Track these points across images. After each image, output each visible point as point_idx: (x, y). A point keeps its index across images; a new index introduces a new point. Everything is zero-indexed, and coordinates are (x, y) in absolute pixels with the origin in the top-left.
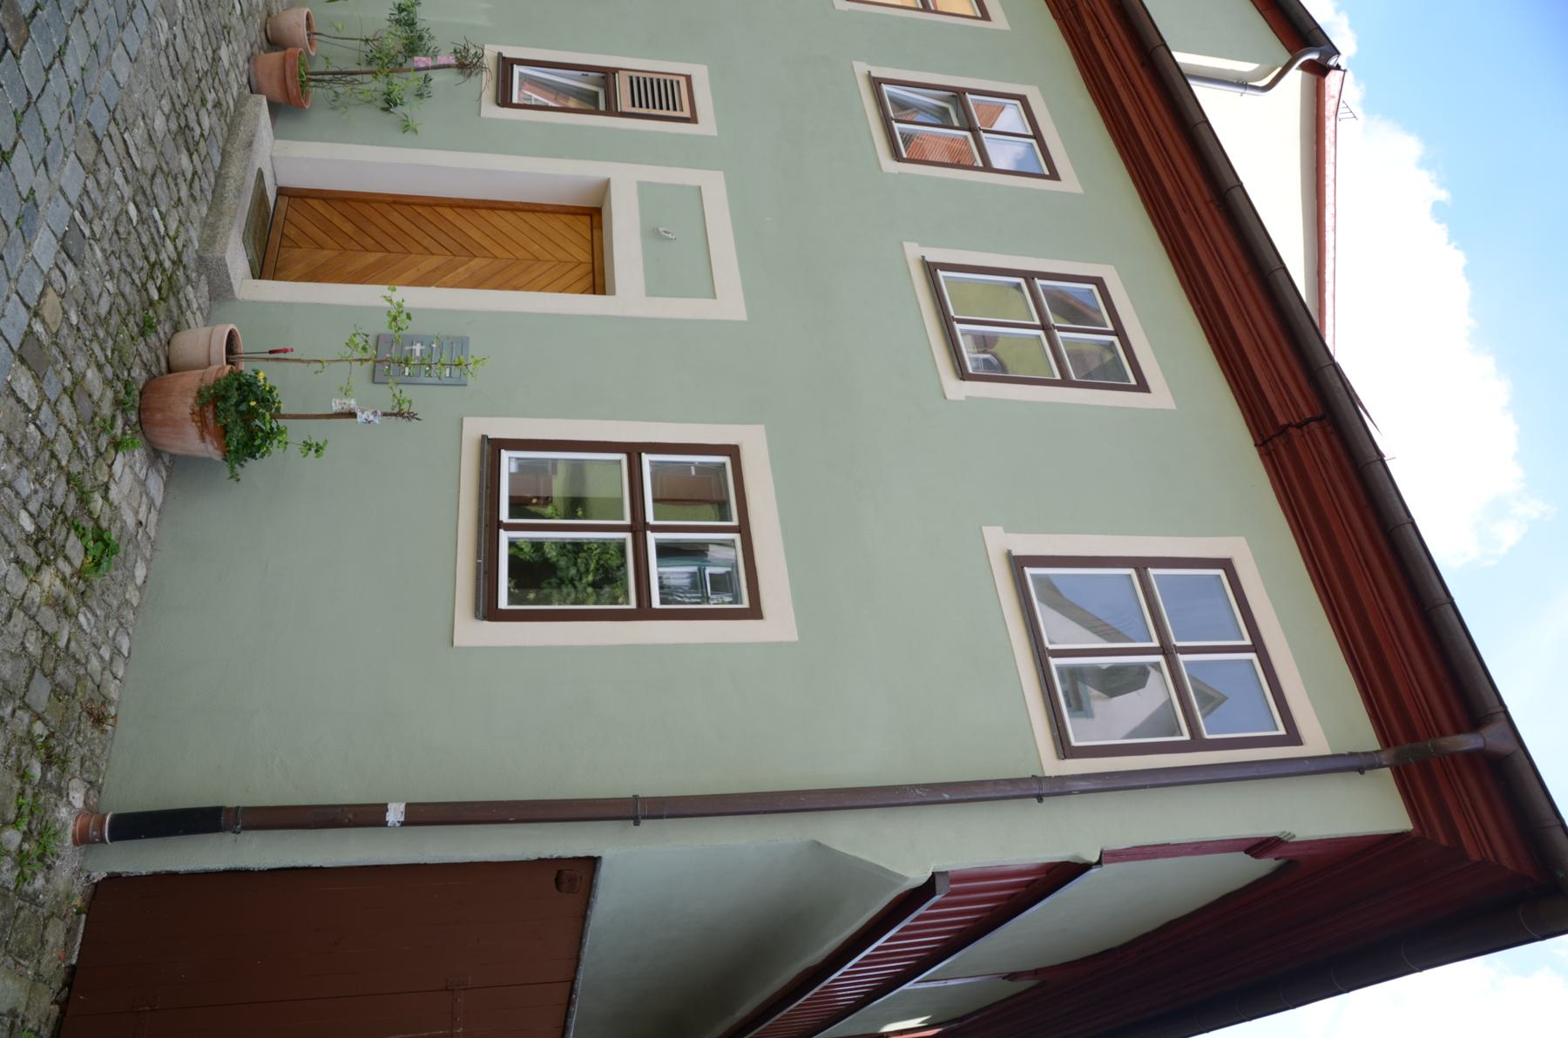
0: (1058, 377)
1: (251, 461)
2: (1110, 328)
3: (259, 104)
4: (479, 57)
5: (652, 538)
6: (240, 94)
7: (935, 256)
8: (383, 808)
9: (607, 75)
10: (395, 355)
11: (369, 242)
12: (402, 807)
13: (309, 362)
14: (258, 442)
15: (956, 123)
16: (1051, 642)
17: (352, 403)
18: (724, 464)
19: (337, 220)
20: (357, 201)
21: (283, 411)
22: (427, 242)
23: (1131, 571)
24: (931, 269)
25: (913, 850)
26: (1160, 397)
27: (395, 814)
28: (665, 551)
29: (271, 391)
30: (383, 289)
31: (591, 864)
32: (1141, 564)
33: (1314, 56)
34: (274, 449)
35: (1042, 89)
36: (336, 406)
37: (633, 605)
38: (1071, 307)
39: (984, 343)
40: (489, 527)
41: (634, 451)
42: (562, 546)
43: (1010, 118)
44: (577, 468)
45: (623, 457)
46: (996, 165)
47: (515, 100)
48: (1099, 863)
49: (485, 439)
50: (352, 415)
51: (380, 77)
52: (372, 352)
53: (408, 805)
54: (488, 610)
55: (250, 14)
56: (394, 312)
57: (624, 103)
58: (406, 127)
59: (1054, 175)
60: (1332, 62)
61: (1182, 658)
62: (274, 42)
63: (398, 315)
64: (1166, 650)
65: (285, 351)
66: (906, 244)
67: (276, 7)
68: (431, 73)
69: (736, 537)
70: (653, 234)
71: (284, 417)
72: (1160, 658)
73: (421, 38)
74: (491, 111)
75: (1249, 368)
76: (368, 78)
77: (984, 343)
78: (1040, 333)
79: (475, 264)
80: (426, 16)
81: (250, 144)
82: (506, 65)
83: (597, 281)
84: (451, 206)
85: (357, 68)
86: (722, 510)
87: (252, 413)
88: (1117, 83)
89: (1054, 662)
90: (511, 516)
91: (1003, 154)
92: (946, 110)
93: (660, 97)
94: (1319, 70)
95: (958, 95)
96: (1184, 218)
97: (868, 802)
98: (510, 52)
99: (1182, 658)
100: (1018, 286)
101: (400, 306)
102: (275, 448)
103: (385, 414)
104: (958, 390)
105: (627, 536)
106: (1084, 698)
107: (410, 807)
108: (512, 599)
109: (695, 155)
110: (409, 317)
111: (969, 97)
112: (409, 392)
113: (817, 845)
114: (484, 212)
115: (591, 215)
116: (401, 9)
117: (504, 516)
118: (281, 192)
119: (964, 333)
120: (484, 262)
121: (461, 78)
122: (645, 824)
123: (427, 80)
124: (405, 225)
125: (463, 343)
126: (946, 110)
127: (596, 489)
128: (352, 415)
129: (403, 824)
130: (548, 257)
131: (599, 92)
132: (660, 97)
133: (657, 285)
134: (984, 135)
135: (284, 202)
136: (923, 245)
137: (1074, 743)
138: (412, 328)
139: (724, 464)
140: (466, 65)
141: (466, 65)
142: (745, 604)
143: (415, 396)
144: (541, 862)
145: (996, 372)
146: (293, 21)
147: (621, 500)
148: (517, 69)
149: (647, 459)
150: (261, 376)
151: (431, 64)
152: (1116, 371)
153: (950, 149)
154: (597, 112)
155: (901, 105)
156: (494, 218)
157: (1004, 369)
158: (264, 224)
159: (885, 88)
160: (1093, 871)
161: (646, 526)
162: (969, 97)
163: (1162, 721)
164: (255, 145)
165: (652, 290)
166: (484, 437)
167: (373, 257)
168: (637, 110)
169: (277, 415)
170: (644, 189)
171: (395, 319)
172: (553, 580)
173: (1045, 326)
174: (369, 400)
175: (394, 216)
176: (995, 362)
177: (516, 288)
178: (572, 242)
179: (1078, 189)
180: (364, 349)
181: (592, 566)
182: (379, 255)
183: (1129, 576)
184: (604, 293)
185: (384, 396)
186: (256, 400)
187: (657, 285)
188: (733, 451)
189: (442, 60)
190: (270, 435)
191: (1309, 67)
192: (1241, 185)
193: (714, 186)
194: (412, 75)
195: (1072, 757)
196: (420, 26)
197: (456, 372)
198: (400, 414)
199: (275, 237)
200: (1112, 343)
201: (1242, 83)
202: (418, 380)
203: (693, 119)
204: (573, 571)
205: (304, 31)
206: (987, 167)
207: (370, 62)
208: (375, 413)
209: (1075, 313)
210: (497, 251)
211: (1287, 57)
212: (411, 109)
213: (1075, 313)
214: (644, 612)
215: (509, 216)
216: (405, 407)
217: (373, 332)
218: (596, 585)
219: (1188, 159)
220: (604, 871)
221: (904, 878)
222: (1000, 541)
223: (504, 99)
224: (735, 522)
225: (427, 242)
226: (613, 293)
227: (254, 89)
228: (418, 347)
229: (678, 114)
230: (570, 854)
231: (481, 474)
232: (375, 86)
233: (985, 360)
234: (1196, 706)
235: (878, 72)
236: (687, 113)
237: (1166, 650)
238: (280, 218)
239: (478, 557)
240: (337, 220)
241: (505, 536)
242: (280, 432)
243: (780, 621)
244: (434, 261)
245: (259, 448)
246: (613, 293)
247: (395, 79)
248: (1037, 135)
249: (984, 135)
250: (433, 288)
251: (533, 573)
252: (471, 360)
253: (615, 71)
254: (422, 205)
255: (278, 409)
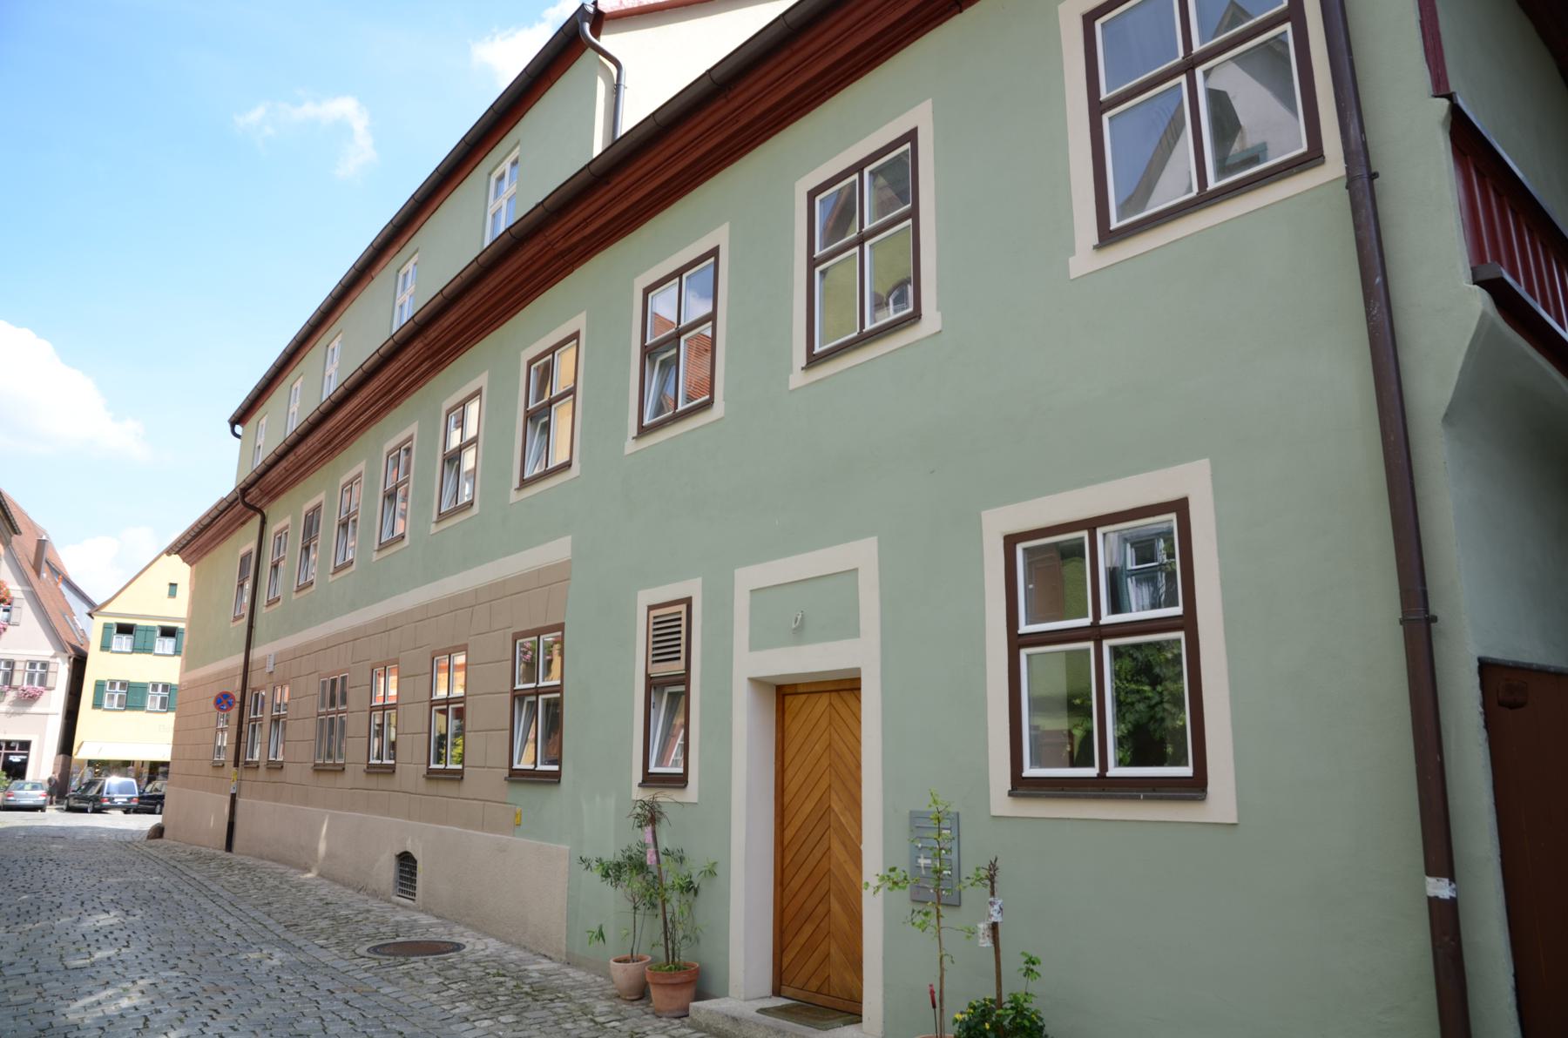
0: (909, 222)
1: (1047, 1030)
2: (856, 177)
3: (698, 1010)
4: (644, 804)
5: (1107, 619)
6: (689, 1027)
7: (800, 358)
8: (1434, 902)
9: (653, 684)
10: (931, 884)
11: (821, 910)
12: (1431, 880)
13: (942, 969)
14: (1027, 1023)
15: (674, 351)
16: (1190, 189)
17: (983, 927)
18: (1025, 550)
19: (802, 939)
20: (782, 921)
21: (994, 997)
22: (817, 854)
23: (1105, 118)
24: (813, 360)
25: (1447, 305)
26: (920, 117)
27: (1441, 889)
28: (1117, 606)
29: (974, 1008)
30: (867, 895)
31: (1487, 669)
32: (1097, 108)
33: (587, 26)
34: (1033, 1007)
35: (636, 275)
36: (986, 943)
37: (1181, 635)
38: (839, 218)
39: (879, 304)
40: (1104, 787)
41: (1016, 642)
42: (1120, 717)
43: (664, 305)
44: (1035, 704)
45: (1024, 653)
46: (709, 309)
47: (680, 770)
48: (1450, 97)
49: (1013, 793)
50: (994, 927)
51: (667, 896)
52: (930, 907)
53: (1429, 874)
54: (1196, 787)
55: (619, 1013)
56: (890, 884)
57: (677, 667)
58: (711, 873)
59: (714, 252)
60: (591, 9)
61: (1197, 47)
62: (641, 993)
63: (892, 881)
64: (1188, 67)
65: (932, 992)
66: (791, 387)
67: (610, 991)
68: (661, 849)
69: (1100, 532)
70: (800, 633)
71: (999, 995)
72: (1199, 72)
73: (630, 858)
74: (692, 793)
75: (883, 32)
76: (668, 907)
77: (879, 304)
78: (867, 245)
79: (836, 807)
80: (612, 854)
81: (735, 1019)
82: (649, 780)
83: (847, 686)
84: (783, 830)
85: (661, 918)
86: (1073, 552)
87: (997, 1027)
88: (625, 204)
89: (1212, 184)
90: (1092, 765)
91: (697, 308)
92: (663, 363)
93: (670, 633)
94: (599, 20)
95: (648, 353)
96: (744, 121)
97: (1392, 366)
98: (638, 776)
99: (1197, 47)
100: (823, 273)
101: (882, 879)
102: (1032, 1006)
103: (993, 894)
104: (931, 319)
105: (1107, 644)
106: (1245, 156)
107: (1432, 870)
108: (1180, 761)
109: (721, 599)
110: (893, 870)
111: (649, 342)
112: (968, 870)
113: (1448, 418)
114: (787, 799)
115: (784, 695)
116: (606, 875)
117: (1092, 772)
118: (777, 992)
119: (874, 320)
120: (834, 796)
121: (664, 821)
122: (1434, 609)
123: (667, 853)
124: (803, 874)
125: (914, 816)
126: (663, 363)
127: (1057, 684)
128: (994, 927)
129: (1452, 879)
130: (826, 735)
131: (668, 691)
132: (670, 633)
133: (848, 627)
134: (683, 324)
135: (787, 990)
136: (790, 370)
137: (1304, 148)
138: (903, 866)
139: (1025, 550)
140: (651, 816)
141: (651, 816)
142: (1173, 516)
143: (972, 862)
144: (1488, 725)
145: (907, 287)
146: (623, 974)
147: (1068, 652)
148: (652, 769)
149: (1024, 628)
150: (959, 1017)
151: (652, 849)
152: (897, 170)
153: (699, 353)
154: (687, 693)
155: (660, 409)
156: (792, 788)
157: (907, 282)
158: (808, 1010)
159: (646, 422)
160: (1461, 102)
161: (1096, 624)
162: (649, 342)
163: (1270, 65)
164: (736, 1014)
165: (853, 631)
166: (1010, 794)
167: (835, 906)
168: (683, 655)
169: (998, 1002)
170: (755, 645)
171: (895, 883)
172: (1152, 726)
173: (860, 241)
174: (977, 912)
175: (795, 884)
176: (896, 293)
177: (859, 767)
178: (810, 712)
179: (725, 228)
180: (926, 914)
181: (1133, 686)
182: (832, 899)
183: (1110, 119)
184: (859, 680)
185: (973, 895)
186: (983, 1023)
187: (848, 627)
188: (1011, 541)
189: (649, 838)
190: (1019, 1011)
191: (596, 32)
192: (709, 71)
193: (748, 578)
194: (664, 868)
195: (1321, 148)
196: (619, 858)
197: (946, 823)
198: (992, 878)
199: (820, 999)
200: (871, 173)
201: (616, 90)
202: (955, 863)
203: (688, 602)
204: (1141, 707)
205: (630, 966)
206: (712, 317)
207: (654, 906)
208: (992, 904)
209: (844, 214)
210: (823, 785)
211: (590, 52)
212: (694, 867)
213: (844, 214)
214: (1188, 623)
215: (789, 774)
216: (984, 873)
217: (909, 906)
218: (1155, 681)
219: (689, 126)
220: (1496, 654)
221: (1484, 315)
222: (1085, 258)
223: (680, 781)
224: (1085, 534)
225: (817, 854)
226: (858, 670)
227: (684, 1014)
228: (922, 862)
229: (684, 616)
230: (1477, 692)
231: (1048, 796)
232: (675, 902)
233: (895, 303)
234: (1251, 22)
235: (633, 430)
236: (683, 608)
237: (1188, 67)
238: (801, 995)
239: (1138, 798)
240: (802, 939)
241: (1114, 771)
242: (1015, 999)
243: (1190, 480)
244: (836, 846)
245: (1031, 1020)
246: (858, 670)
247: (668, 882)
248: (678, 273)
249: (683, 324)
250: (863, 847)
251: (1145, 743)
252: (934, 809)
253: (648, 678)
254: (783, 858)
255: (991, 1001)
